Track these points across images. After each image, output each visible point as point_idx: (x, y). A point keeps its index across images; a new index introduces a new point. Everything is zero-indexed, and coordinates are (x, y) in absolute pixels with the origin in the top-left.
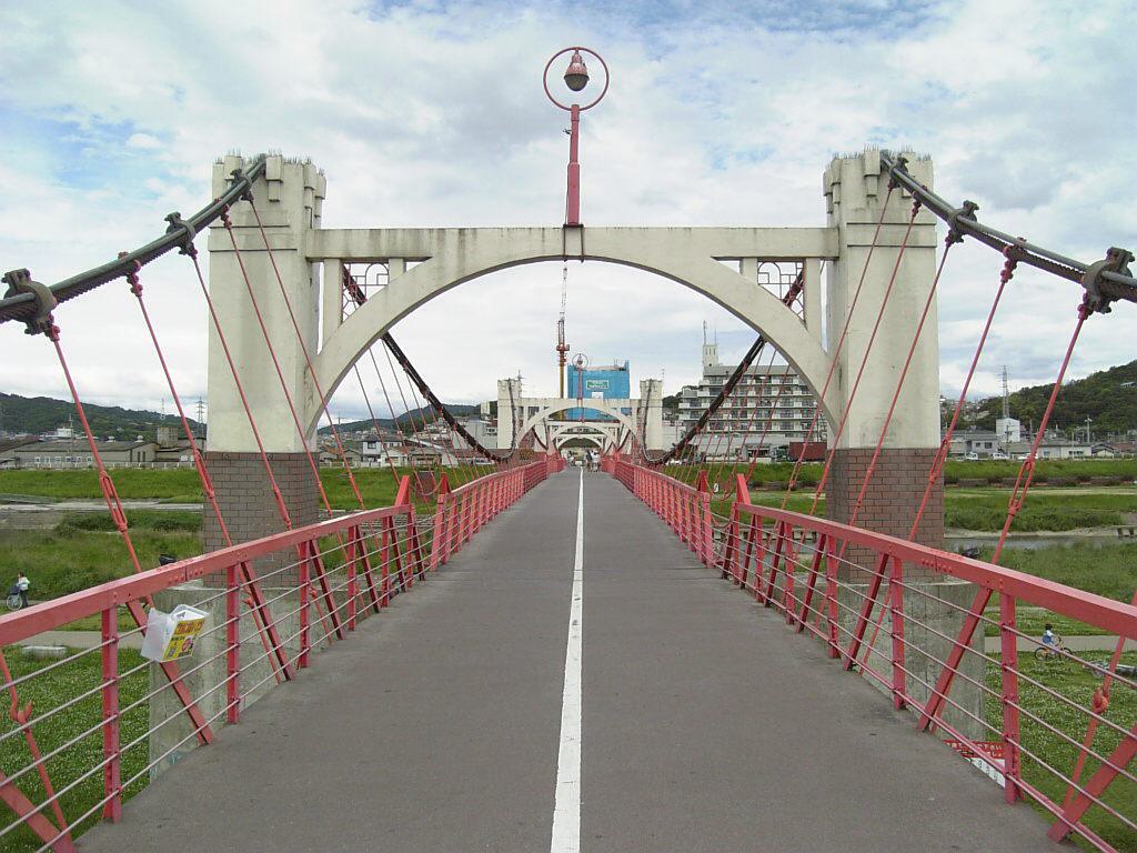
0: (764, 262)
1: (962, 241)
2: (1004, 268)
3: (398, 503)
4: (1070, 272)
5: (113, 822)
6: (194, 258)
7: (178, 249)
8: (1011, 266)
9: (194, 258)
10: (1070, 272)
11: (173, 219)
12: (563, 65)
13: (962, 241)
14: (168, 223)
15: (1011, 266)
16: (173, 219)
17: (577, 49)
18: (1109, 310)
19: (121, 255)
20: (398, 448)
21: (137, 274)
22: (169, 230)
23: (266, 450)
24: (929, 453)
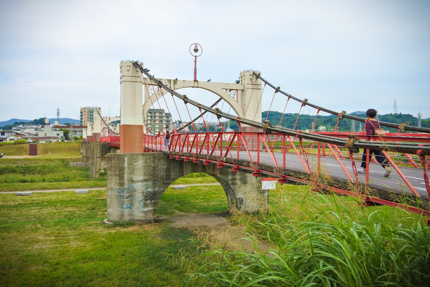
4: (300, 101)
5: (144, 176)
8: (289, 98)
10: (300, 101)
12: (193, 47)
15: (289, 98)
17: (196, 44)
18: (264, 115)
20: (14, 135)
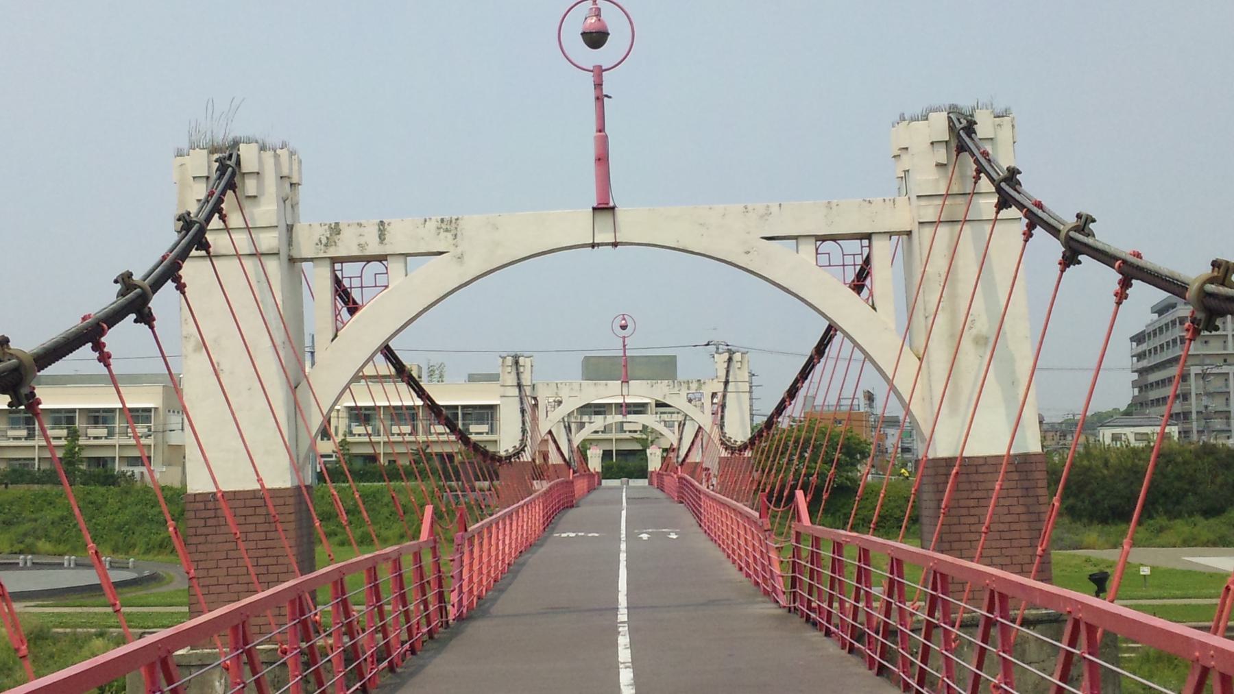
0: (824, 241)
1: (1079, 262)
2: (1118, 287)
3: (424, 535)
6: (152, 327)
7: (133, 316)
9: (152, 327)
11: (126, 280)
12: (579, 21)
13: (1079, 262)
14: (118, 287)
16: (126, 280)
17: (623, 315)
19: (84, 319)
21: (103, 339)
22: (121, 294)
23: (268, 486)
24: (982, 462)
